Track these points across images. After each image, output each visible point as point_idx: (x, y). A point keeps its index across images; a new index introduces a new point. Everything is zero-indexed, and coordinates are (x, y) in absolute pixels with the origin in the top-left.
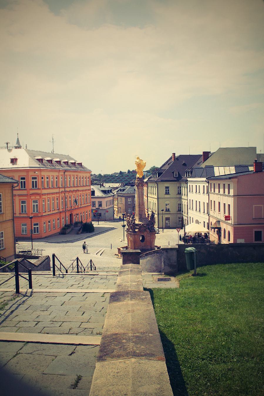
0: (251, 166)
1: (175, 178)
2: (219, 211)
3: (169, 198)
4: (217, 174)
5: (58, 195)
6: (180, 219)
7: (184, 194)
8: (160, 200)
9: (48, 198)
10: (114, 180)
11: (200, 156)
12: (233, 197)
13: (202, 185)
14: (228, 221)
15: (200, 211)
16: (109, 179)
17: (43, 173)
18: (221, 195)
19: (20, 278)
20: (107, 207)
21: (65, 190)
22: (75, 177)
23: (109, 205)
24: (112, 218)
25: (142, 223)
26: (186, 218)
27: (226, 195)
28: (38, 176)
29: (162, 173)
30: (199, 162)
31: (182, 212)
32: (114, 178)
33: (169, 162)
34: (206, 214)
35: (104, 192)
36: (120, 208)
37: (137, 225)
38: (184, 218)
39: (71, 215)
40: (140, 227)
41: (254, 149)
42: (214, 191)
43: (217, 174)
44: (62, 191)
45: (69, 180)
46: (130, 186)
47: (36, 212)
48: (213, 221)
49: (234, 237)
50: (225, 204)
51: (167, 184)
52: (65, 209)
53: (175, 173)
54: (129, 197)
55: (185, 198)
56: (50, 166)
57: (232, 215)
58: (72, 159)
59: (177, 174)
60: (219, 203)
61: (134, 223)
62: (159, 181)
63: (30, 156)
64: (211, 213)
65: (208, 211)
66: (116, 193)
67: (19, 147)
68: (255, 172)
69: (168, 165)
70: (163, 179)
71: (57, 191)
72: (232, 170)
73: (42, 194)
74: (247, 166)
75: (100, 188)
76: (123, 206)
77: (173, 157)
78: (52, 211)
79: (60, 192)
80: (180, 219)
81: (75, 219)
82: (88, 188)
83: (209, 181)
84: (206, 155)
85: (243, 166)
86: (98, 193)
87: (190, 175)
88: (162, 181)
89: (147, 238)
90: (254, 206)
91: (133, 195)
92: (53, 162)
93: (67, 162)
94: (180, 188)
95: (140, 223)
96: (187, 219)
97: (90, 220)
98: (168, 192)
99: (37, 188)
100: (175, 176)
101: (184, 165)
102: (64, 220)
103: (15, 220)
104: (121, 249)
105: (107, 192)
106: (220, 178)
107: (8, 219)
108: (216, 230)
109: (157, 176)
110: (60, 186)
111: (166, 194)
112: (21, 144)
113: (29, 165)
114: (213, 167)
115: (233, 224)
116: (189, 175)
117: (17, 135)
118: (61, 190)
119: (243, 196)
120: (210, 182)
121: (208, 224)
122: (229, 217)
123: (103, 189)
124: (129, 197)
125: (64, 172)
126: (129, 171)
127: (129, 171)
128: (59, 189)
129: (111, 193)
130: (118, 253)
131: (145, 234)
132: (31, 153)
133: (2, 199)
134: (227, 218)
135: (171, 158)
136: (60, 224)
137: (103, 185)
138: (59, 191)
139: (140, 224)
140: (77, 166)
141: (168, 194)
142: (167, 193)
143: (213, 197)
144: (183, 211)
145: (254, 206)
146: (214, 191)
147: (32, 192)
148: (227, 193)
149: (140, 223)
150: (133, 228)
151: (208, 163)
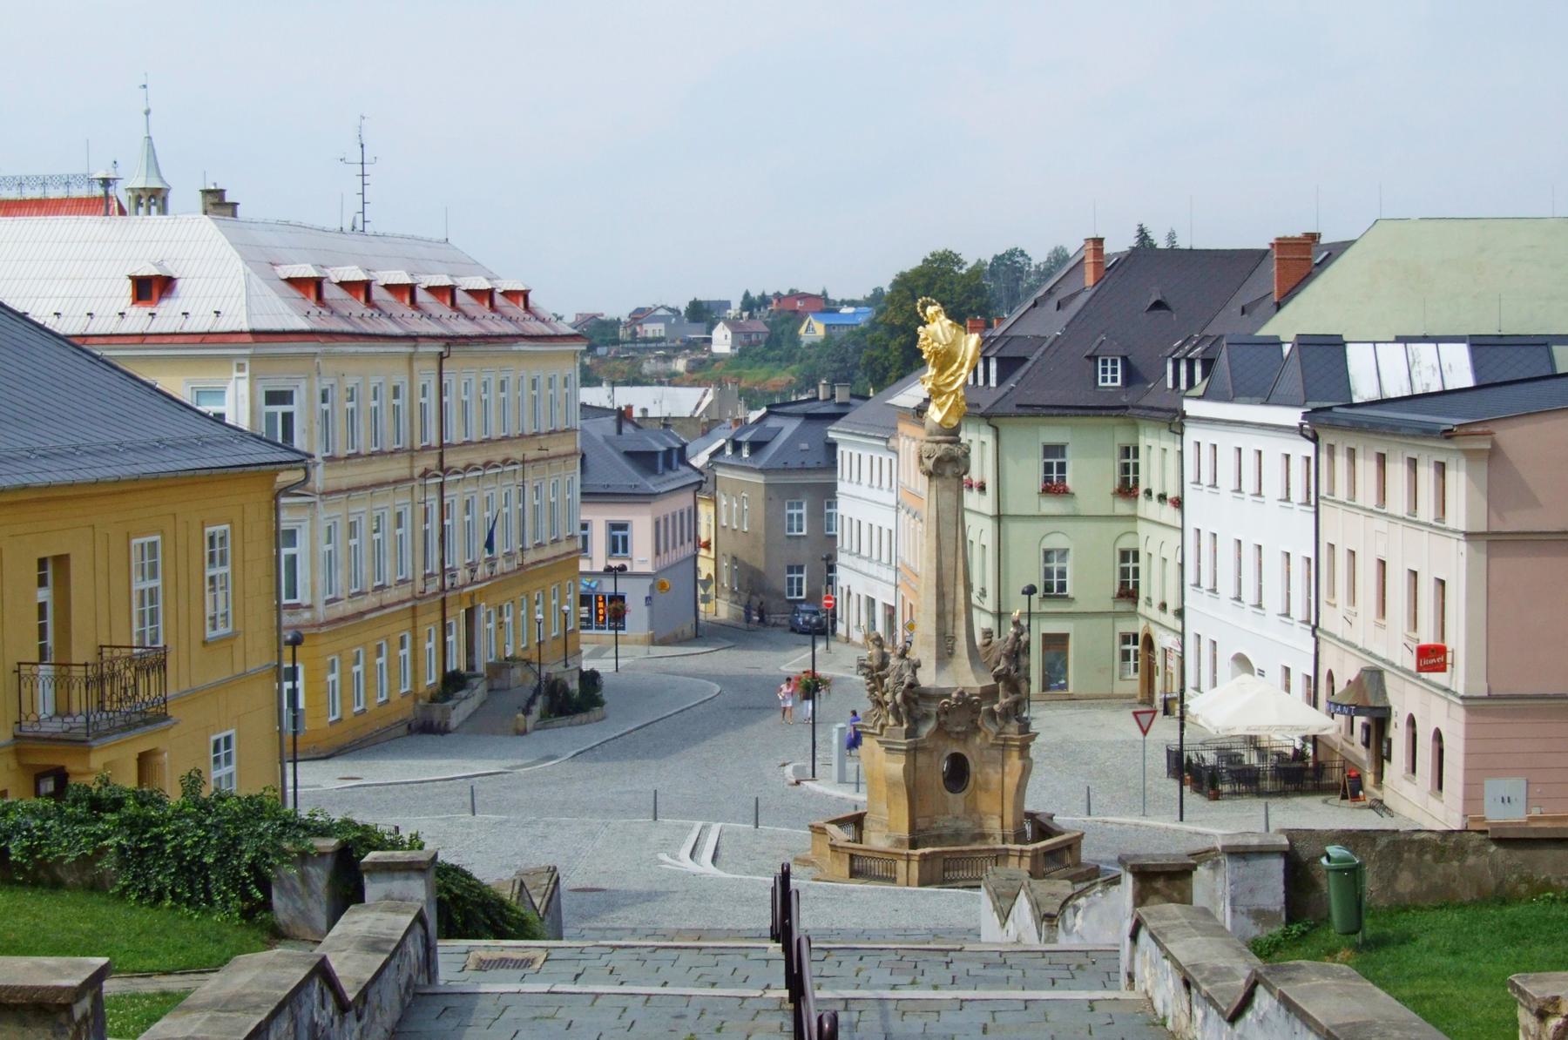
2: (1352, 600)
4: (1364, 389)
6: (1131, 647)
8: (1014, 530)
12: (1461, 536)
13: (1273, 447)
24: (688, 629)
29: (1024, 360)
30: (1245, 296)
43: (1364, 389)
48: (1347, 670)
49: (1467, 770)
51: (1053, 433)
53: (1104, 363)
58: (474, 267)
59: (1104, 371)
61: (911, 686)
62: (1007, 411)
63: (247, 261)
69: (1059, 307)
77: (1090, 260)
96: (1179, 649)
103: (1321, 507)
105: (660, 460)
107: (253, 665)
113: (249, 316)
116: (1191, 383)
120: (1326, 438)
121: (1313, 682)
122: (1440, 651)
129: (684, 469)
134: (1432, 657)
142: (1054, 487)
143: (1341, 527)
148: (1427, 511)
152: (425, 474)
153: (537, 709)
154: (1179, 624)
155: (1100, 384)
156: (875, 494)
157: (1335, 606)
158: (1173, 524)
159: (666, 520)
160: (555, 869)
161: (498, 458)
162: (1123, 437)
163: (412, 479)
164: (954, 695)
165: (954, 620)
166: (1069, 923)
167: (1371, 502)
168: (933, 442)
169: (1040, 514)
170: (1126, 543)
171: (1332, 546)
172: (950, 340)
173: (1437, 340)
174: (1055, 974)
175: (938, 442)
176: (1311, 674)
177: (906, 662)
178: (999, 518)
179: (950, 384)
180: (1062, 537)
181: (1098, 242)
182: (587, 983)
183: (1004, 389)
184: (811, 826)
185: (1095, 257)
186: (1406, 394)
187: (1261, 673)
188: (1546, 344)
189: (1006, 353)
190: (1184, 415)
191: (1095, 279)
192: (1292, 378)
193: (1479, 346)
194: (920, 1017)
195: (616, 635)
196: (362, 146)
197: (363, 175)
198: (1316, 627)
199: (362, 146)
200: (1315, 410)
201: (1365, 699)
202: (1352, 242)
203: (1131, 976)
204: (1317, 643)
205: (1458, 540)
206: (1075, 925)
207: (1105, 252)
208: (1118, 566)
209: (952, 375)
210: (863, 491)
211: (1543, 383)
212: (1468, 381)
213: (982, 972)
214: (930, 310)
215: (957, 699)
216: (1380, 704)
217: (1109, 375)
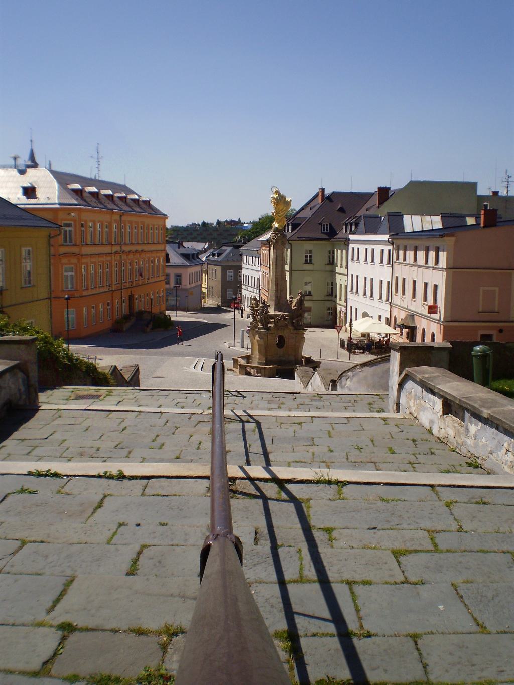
0: (470, 216)
1: (324, 233)
3: (312, 271)
4: (408, 229)
5: (109, 259)
7: (339, 265)
9: (99, 262)
10: (192, 237)
11: (370, 195)
13: (378, 249)
14: (433, 315)
15: (372, 296)
16: (211, 234)
17: (84, 216)
18: (419, 266)
19: (327, 614)
20: (192, 285)
21: (121, 247)
22: (134, 225)
23: (192, 283)
24: (199, 308)
25: (280, 313)
26: (343, 309)
27: (429, 268)
28: (75, 221)
29: (300, 224)
30: (368, 205)
31: (333, 298)
32: (191, 234)
33: (312, 204)
34: (385, 302)
35: (186, 256)
36: (213, 288)
37: (272, 316)
38: (339, 307)
39: (131, 298)
40: (278, 320)
41: (474, 185)
42: (405, 259)
43: (408, 229)
44: (117, 252)
45: (128, 229)
46: (232, 248)
47: (69, 289)
48: (401, 316)
50: (426, 284)
51: (308, 246)
52: (121, 284)
54: (230, 268)
55: (341, 272)
56: (95, 202)
57: (441, 303)
58: (133, 193)
60: (414, 282)
62: (294, 239)
64: (396, 300)
65: (388, 295)
66: (205, 258)
67: (34, 165)
68: (484, 227)
70: (301, 236)
71: (107, 249)
72: (436, 222)
73: (82, 255)
74: (463, 217)
75: (177, 250)
76: (217, 284)
77: (320, 195)
78: (90, 289)
79: (113, 252)
80: (330, 311)
81: (137, 307)
82: (160, 247)
83: (394, 241)
84: (384, 193)
85: (457, 215)
86: (175, 259)
87: (353, 229)
88: (300, 239)
89: (289, 342)
90: (482, 289)
91: (237, 264)
92: (100, 197)
93: (125, 198)
94: (332, 254)
95: (278, 313)
97: (163, 307)
98: (310, 261)
99: (73, 243)
100: (324, 230)
101: (342, 210)
102: (121, 308)
103: (394, 265)
104: (240, 360)
105: (191, 256)
106: (414, 235)
107: (41, 297)
108: (405, 331)
109: (290, 229)
110: (113, 243)
111: (306, 263)
112: (38, 160)
114: (402, 216)
115: (442, 320)
117: (30, 142)
118: (115, 249)
119: (463, 270)
120: (396, 242)
122: (436, 307)
123: (182, 251)
124: (230, 268)
125: (121, 216)
126: (219, 223)
127: (219, 223)
128: (112, 247)
130: (234, 368)
131: (285, 333)
132: (62, 178)
133: (68, 222)
134: (432, 309)
135: (316, 196)
136: (113, 313)
137: (182, 244)
138: (112, 250)
139: (278, 315)
140: (143, 206)
141: (310, 263)
142: (308, 261)
144: (336, 296)
145: (482, 289)
146: (405, 259)
147: (63, 250)
149: (278, 313)
150: (263, 321)
151: (390, 206)
152: (116, 253)
153: (150, 326)
154: (345, 304)
156: (254, 268)
158: (344, 273)
159: (192, 274)
160: (138, 365)
161: (140, 250)
163: (112, 253)
166: (343, 383)
167: (412, 262)
174: (345, 405)
176: (389, 317)
182: (123, 405)
183: (294, 232)
184: (233, 359)
186: (420, 230)
187: (372, 317)
189: (294, 222)
190: (349, 240)
192: (385, 226)
194: (291, 426)
195: (243, 429)
198: (390, 303)
200: (393, 235)
203: (398, 405)
204: (391, 307)
205: (443, 271)
206: (346, 384)
210: (250, 267)
212: (440, 226)
213: (311, 403)
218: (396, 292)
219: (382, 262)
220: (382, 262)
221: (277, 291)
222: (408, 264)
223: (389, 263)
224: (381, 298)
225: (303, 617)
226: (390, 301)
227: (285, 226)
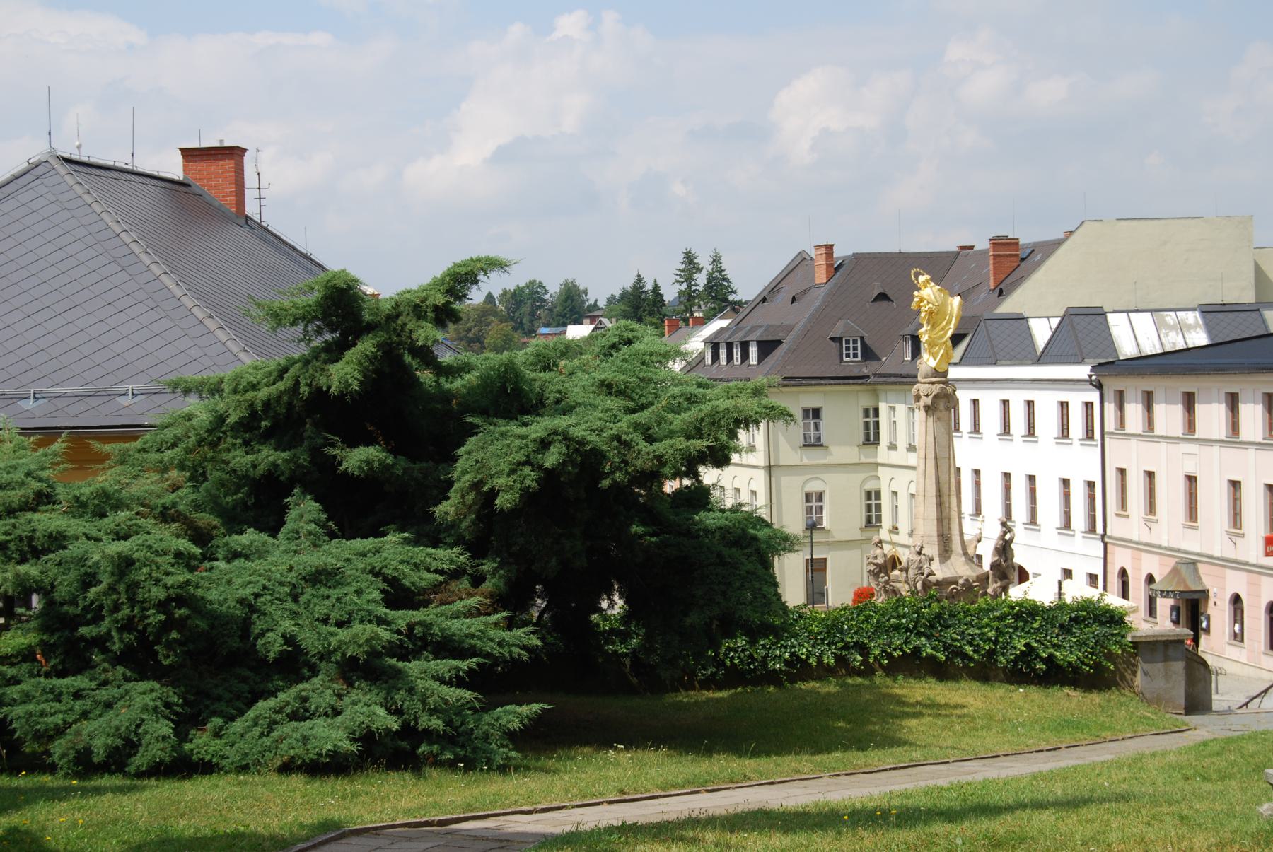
29: (779, 342)
53: (848, 342)
59: (848, 349)
64: (1129, 526)
83: (1105, 381)
155: (845, 359)
157: (1128, 517)
162: (866, 401)
164: (961, 581)
165: (949, 524)
167: (1178, 428)
168: (929, 383)
169: (801, 463)
170: (871, 486)
171: (1122, 472)
172: (940, 302)
173: (1175, 310)
175: (933, 383)
177: (923, 557)
178: (769, 469)
179: (942, 337)
180: (819, 482)
181: (829, 248)
185: (827, 260)
188: (1258, 310)
191: (827, 277)
193: (1209, 312)
196: (259, 174)
197: (260, 198)
199: (259, 174)
200: (1100, 364)
201: (1186, 585)
202: (1058, 243)
207: (835, 256)
208: (864, 503)
209: (943, 329)
211: (1229, 345)
214: (922, 279)
215: (963, 585)
216: (1200, 588)
217: (851, 352)
218: (1123, 504)
219: (1065, 432)
220: (1065, 432)
221: (942, 521)
222: (1162, 437)
223: (1089, 434)
224: (1067, 524)
225: (117, 164)
226: (1099, 530)
227: (761, 326)
